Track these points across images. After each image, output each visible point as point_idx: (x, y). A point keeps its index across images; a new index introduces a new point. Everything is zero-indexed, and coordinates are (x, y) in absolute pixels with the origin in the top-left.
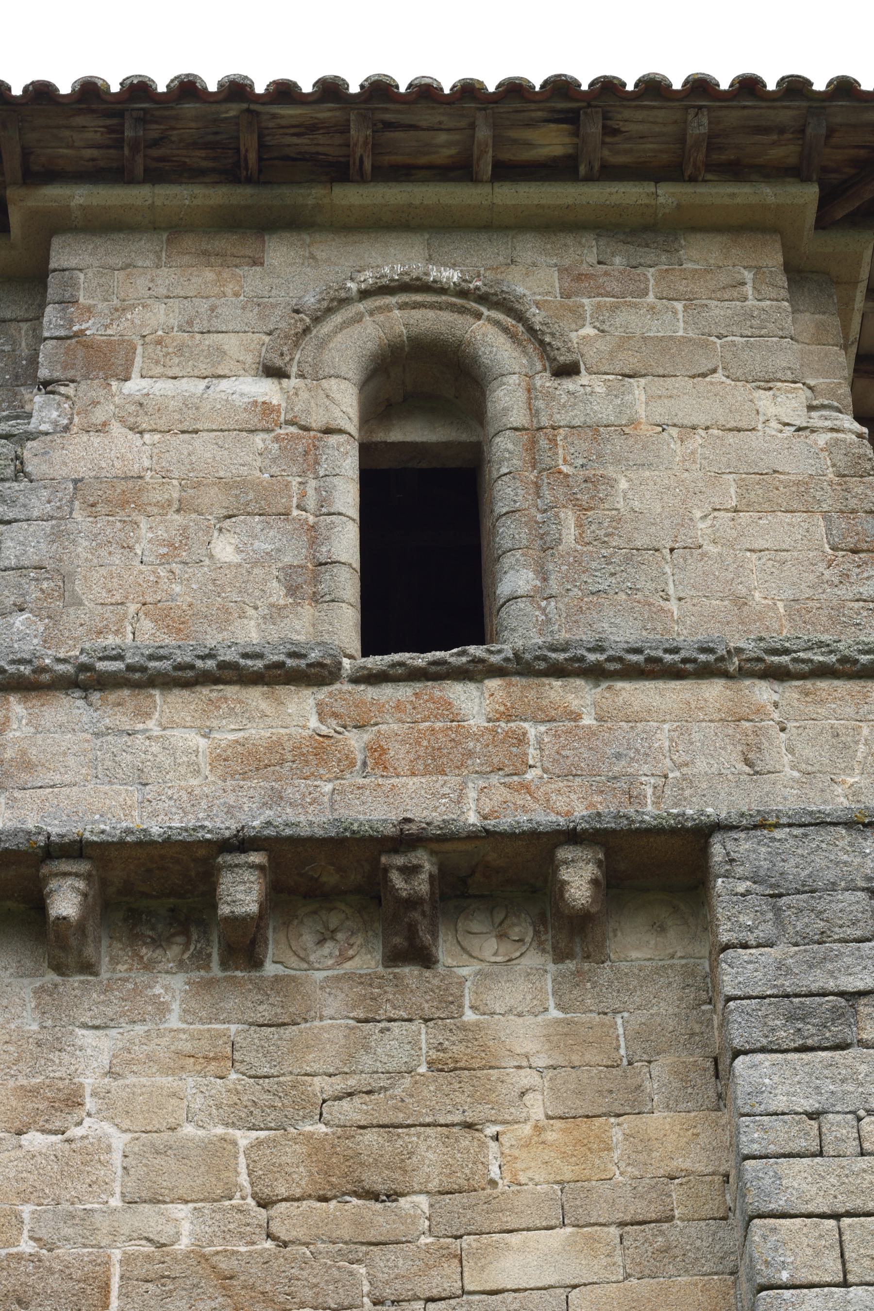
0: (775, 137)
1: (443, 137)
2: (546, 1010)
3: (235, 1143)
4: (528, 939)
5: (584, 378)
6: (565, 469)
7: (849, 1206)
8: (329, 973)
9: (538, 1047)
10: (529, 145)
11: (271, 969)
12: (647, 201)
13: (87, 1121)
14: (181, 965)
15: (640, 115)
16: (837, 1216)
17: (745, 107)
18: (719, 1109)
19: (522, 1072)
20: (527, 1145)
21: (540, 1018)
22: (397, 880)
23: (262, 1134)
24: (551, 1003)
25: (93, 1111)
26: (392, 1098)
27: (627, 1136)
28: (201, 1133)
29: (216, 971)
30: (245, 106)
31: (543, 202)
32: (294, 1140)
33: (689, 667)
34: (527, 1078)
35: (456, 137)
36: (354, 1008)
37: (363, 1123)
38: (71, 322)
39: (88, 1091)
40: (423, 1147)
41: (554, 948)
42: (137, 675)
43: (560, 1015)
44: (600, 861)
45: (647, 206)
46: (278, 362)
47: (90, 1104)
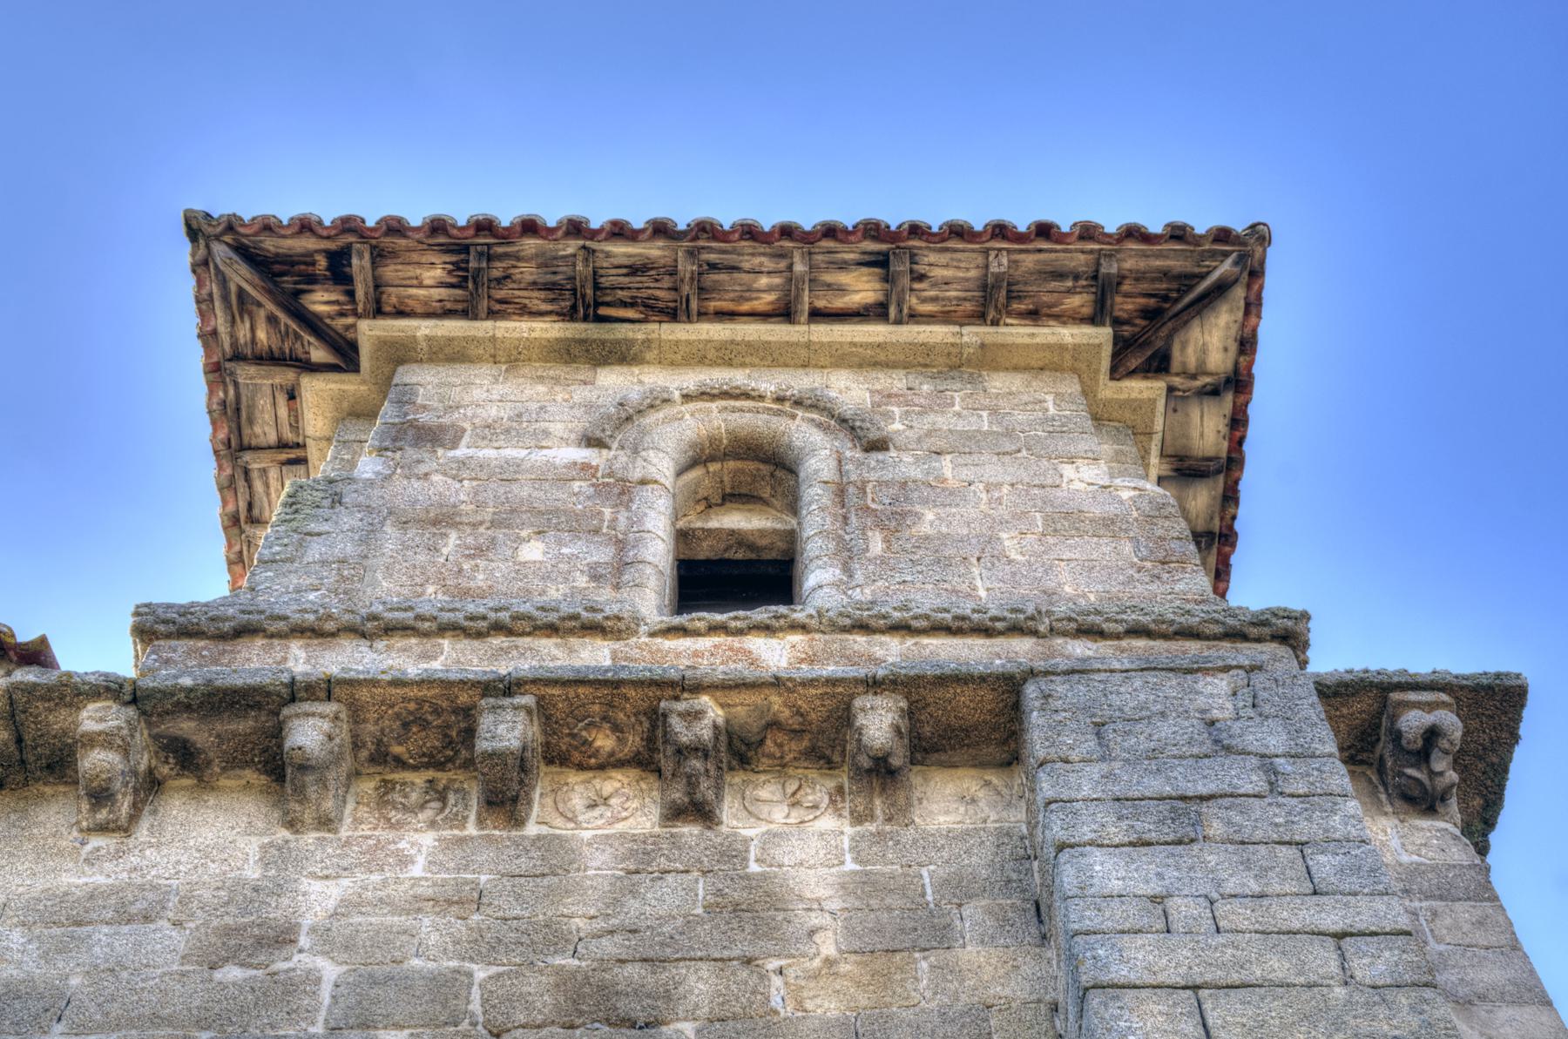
0: (1070, 284)
1: (764, 281)
2: (843, 863)
3: (470, 975)
4: (824, 805)
5: (893, 453)
6: (873, 506)
7: (1208, 977)
8: (600, 832)
9: (831, 893)
10: (842, 290)
11: (532, 829)
12: (951, 340)
13: (296, 958)
14: (432, 824)
15: (943, 258)
16: (1195, 988)
17: (1040, 251)
18: (1043, 945)
19: (813, 914)
20: (816, 976)
21: (834, 870)
22: (676, 724)
23: (501, 969)
24: (848, 857)
25: (307, 946)
26: (659, 934)
27: (932, 967)
28: (431, 965)
29: (471, 830)
30: (581, 242)
31: (856, 340)
32: (541, 972)
33: (999, 625)
34: (815, 919)
35: (777, 280)
36: (623, 860)
37: (623, 957)
38: (406, 414)
39: (305, 929)
40: (693, 978)
41: (852, 813)
42: (427, 624)
43: (858, 868)
44: (902, 710)
45: (952, 345)
46: (598, 434)
47: (304, 941)
